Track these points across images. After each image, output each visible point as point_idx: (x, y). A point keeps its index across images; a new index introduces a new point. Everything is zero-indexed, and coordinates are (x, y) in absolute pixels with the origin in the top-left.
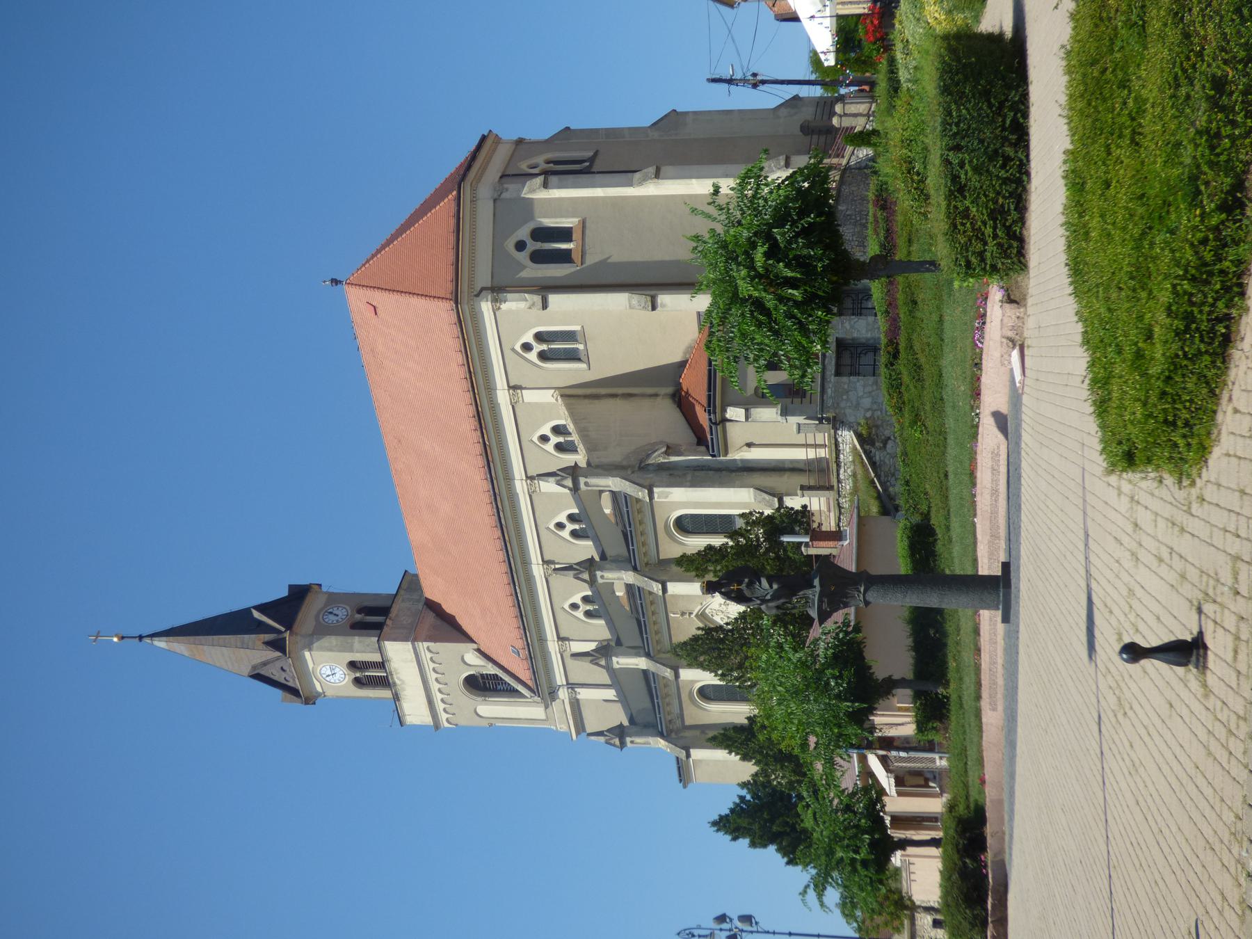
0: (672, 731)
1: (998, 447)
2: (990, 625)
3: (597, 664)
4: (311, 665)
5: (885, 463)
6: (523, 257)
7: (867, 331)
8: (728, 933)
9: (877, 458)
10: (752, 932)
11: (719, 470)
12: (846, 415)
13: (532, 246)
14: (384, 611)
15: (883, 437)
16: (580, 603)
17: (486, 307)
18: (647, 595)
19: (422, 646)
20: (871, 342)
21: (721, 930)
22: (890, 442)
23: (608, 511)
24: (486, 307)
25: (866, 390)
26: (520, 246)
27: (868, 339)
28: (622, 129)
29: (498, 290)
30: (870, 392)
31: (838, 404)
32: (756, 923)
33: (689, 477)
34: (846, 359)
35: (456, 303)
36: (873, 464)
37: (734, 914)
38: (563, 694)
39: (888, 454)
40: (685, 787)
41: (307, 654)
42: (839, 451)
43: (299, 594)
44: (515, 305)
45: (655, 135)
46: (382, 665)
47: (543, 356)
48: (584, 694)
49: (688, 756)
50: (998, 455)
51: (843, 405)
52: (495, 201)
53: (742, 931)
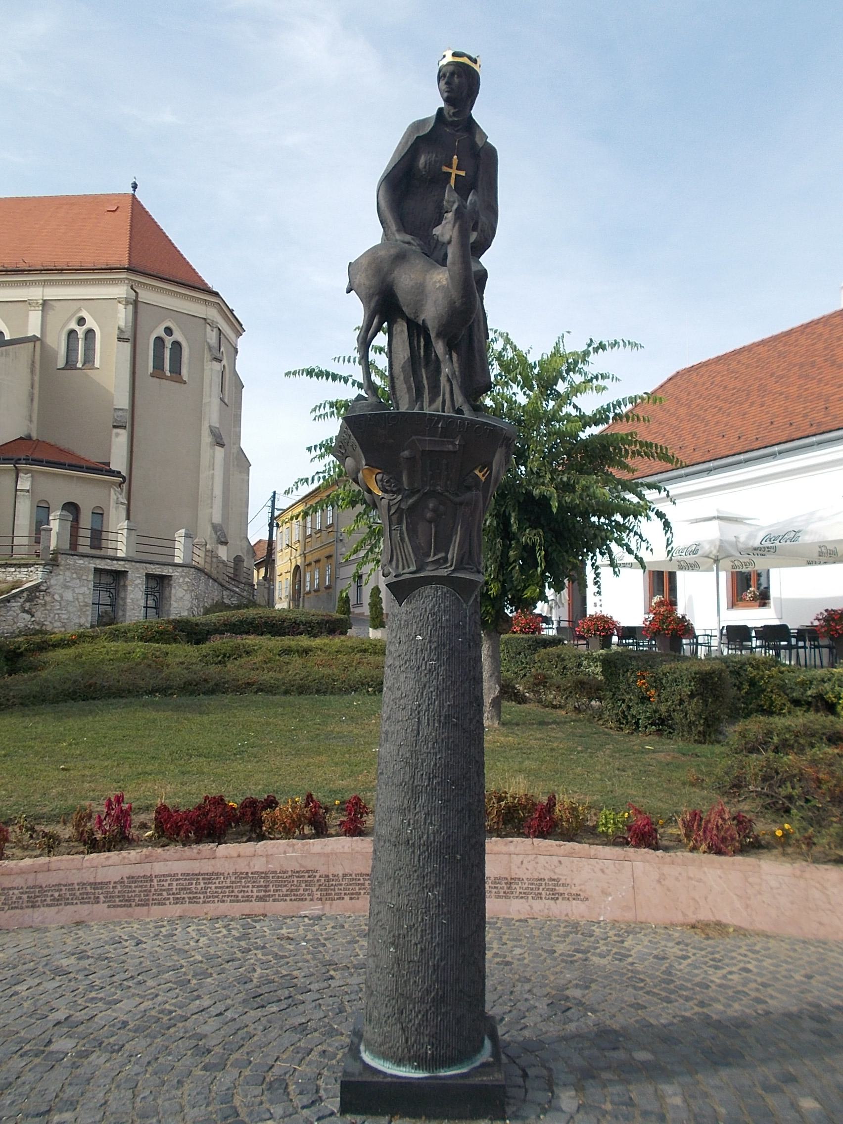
1: (577, 897)
2: (83, 884)
5: (8, 611)
6: (160, 332)
7: (131, 599)
12: (57, 576)
15: (34, 610)
20: (121, 602)
22: (29, 616)
24: (121, 291)
25: (81, 597)
27: (124, 599)
30: (77, 599)
31: (68, 569)
39: (18, 614)
42: (20, 567)
44: (122, 316)
45: (234, 450)
47: (72, 333)
50: (555, 896)
51: (68, 573)
52: (205, 319)
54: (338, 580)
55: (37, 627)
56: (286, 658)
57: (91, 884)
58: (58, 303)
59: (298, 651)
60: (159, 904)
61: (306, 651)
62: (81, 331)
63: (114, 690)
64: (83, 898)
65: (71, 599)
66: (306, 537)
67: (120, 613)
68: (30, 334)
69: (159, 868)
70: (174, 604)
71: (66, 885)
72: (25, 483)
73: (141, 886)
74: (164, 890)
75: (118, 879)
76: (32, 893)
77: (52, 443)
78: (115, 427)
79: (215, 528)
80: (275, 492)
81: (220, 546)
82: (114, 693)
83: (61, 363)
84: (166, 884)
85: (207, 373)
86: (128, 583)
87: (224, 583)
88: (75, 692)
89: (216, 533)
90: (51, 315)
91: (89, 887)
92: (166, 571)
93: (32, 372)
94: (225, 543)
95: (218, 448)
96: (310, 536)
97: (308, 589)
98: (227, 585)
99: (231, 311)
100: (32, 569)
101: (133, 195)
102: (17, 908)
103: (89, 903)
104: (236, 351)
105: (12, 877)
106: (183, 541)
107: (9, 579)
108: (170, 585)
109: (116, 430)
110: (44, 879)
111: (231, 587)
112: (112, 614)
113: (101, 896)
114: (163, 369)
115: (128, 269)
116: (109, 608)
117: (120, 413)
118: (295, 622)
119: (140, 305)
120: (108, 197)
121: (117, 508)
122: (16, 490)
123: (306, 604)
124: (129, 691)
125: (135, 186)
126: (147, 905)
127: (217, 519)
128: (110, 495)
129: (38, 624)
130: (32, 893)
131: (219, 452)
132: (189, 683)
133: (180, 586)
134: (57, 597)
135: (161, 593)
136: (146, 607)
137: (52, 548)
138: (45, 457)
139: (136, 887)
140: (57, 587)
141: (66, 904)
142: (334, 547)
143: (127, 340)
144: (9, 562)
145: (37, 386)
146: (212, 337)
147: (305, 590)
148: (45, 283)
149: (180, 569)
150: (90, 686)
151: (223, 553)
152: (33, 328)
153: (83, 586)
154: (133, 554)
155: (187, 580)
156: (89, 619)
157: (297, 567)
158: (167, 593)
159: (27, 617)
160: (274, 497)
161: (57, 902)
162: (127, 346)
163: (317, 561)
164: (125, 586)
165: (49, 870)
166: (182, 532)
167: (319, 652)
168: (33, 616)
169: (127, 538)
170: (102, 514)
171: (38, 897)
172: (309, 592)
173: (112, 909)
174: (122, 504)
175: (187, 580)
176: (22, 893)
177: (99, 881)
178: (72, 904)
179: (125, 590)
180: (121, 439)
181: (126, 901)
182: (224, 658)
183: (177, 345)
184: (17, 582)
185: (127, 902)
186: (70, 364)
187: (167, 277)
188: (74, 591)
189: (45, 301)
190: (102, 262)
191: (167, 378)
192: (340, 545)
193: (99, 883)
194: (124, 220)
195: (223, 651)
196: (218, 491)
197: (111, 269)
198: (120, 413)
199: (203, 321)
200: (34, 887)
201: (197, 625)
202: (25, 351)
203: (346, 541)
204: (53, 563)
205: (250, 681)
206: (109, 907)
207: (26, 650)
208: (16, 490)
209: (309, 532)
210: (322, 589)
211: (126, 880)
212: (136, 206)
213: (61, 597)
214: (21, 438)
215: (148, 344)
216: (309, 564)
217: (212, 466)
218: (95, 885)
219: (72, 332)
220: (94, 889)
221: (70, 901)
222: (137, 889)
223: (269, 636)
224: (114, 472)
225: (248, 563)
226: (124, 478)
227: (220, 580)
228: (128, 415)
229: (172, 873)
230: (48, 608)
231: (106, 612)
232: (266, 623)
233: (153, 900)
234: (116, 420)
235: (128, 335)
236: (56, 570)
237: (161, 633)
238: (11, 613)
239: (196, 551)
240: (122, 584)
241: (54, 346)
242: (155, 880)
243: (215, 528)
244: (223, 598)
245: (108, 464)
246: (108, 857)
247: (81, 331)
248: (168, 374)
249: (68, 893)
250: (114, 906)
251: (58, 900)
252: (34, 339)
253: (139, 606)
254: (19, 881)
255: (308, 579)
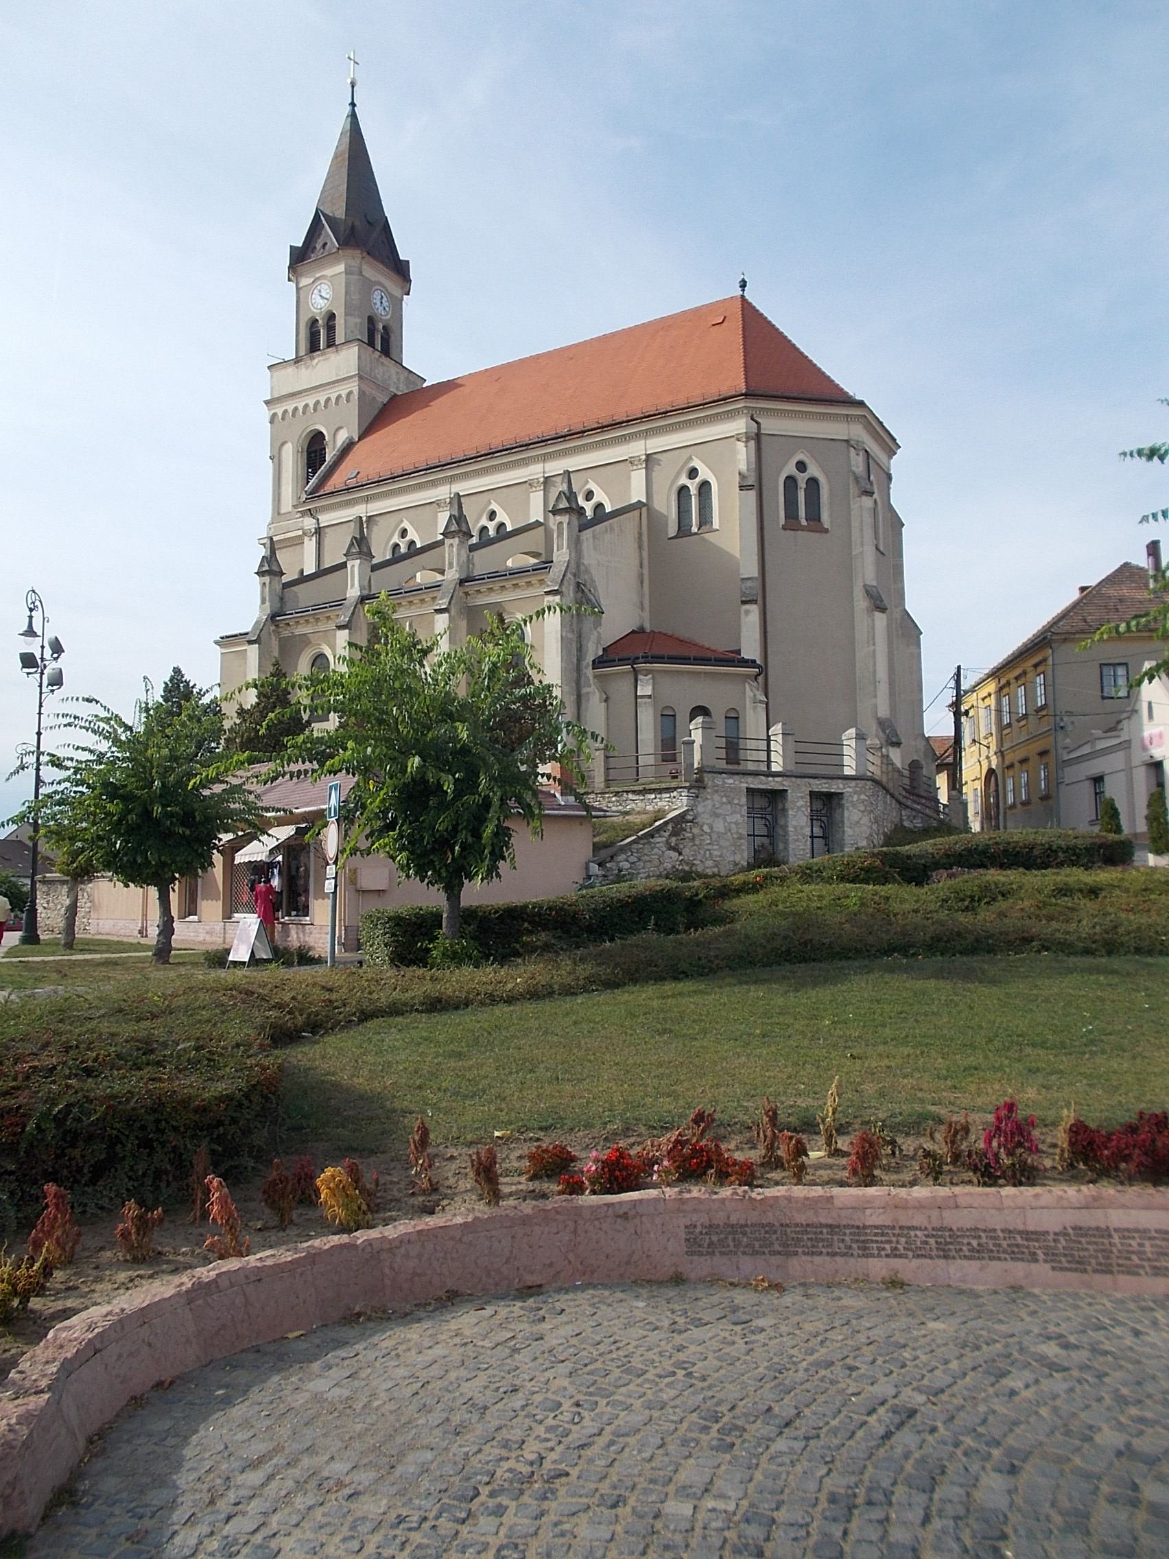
0: (277, 626)
3: (352, 544)
4: (329, 272)
5: (652, 849)
6: (790, 469)
7: (795, 827)
8: (38, 656)
9: (659, 840)
10: (41, 686)
11: (578, 669)
13: (802, 479)
14: (386, 351)
16: (408, 538)
17: (739, 425)
18: (431, 595)
19: (354, 386)
21: (43, 647)
23: (509, 563)
24: (739, 425)
26: (801, 466)
27: (785, 827)
28: (902, 581)
29: (757, 438)
31: (717, 791)
32: (52, 691)
33: (570, 636)
34: (760, 802)
35: (745, 395)
36: (651, 835)
37: (63, 662)
38: (309, 523)
40: (216, 642)
41: (341, 268)
43: (401, 270)
44: (742, 456)
45: (897, 615)
46: (331, 343)
48: (310, 545)
49: (250, 642)
51: (716, 797)
52: (847, 441)
53: (42, 673)
54: (1062, 787)
55: (687, 868)
56: (1065, 901)
57: (1020, 1232)
58: (664, 455)
59: (1081, 891)
60: (1129, 1273)
61: (1093, 892)
62: (693, 486)
63: (838, 949)
64: (1013, 1252)
65: (722, 830)
66: (1001, 728)
67: (781, 846)
68: (634, 501)
69: (1117, 1218)
70: (848, 831)
71: (985, 1231)
72: (645, 689)
73: (1096, 1243)
74: (1133, 1252)
75: (1058, 1229)
76: (941, 1237)
77: (670, 633)
78: (744, 602)
79: (882, 723)
80: (959, 668)
81: (891, 749)
82: (838, 953)
83: (672, 530)
84: (1133, 1243)
85: (855, 512)
86: (788, 805)
87: (901, 798)
88: (788, 951)
89: (884, 731)
90: (657, 473)
91: (1018, 1237)
92: (835, 787)
93: (640, 547)
94: (897, 744)
95: (878, 615)
96: (1009, 725)
97: (1010, 800)
98: (904, 800)
99: (881, 423)
100: (675, 793)
101: (743, 296)
102: (925, 1256)
103: (1022, 1260)
104: (889, 477)
105: (910, 1212)
106: (853, 744)
107: (649, 808)
108: (841, 806)
109: (747, 607)
110: (953, 1219)
111: (909, 803)
112: (770, 848)
113: (1039, 1252)
114: (797, 517)
115: (746, 395)
116: (766, 841)
117: (749, 584)
118: (1050, 849)
119: (764, 439)
120: (711, 307)
121: (755, 708)
122: (636, 697)
123: (1009, 824)
124: (857, 951)
125: (743, 285)
126: (1111, 1272)
127: (883, 711)
128: (744, 693)
129: (687, 864)
130: (941, 1237)
131: (880, 619)
132: (937, 939)
133: (854, 806)
134: (706, 828)
135: (830, 816)
136: (812, 837)
137: (696, 766)
138: (666, 652)
139: (1088, 1243)
140: (706, 816)
141: (991, 1259)
142: (1051, 739)
143: (750, 487)
144: (648, 787)
145: (646, 563)
146: (858, 463)
147: (1005, 803)
148: (647, 434)
149: (853, 783)
150: (805, 943)
151: (896, 755)
152: (637, 494)
153: (735, 812)
154: (792, 767)
155: (863, 797)
156: (745, 855)
157: (991, 772)
158: (837, 816)
159: (674, 854)
160: (958, 674)
161: (977, 1253)
162: (752, 495)
163: (1024, 761)
164: (784, 810)
165: (957, 1207)
166: (852, 732)
167: (1118, 892)
168: (680, 854)
169: (783, 746)
170: (737, 718)
171: (951, 1243)
172: (1013, 806)
173: (1058, 1273)
174: (761, 702)
175: (863, 797)
176: (927, 1236)
177: (1031, 1228)
178: (999, 1259)
179: (785, 815)
180: (751, 617)
181: (1078, 1262)
182: (972, 902)
183: (813, 482)
184: (659, 811)
185: (1079, 1265)
186: (683, 530)
187: (795, 395)
188: (725, 820)
189: (648, 456)
190: (713, 392)
191: (803, 529)
192: (1060, 735)
193: (1032, 1233)
194: (733, 334)
195: (969, 893)
196: (882, 673)
197: (725, 399)
198: (749, 584)
199: (845, 444)
200: (942, 1229)
201: (909, 857)
202: (631, 519)
203: (1070, 728)
204: (698, 785)
205: (1026, 935)
206: (1053, 1269)
207: (705, 897)
208: (636, 697)
209: (1006, 720)
210: (1035, 799)
211: (1070, 1231)
212: (747, 308)
213: (711, 828)
214: (633, 632)
215: (777, 488)
216: (1011, 766)
217: (872, 640)
218: (1027, 1235)
219: (683, 489)
220: (1027, 1240)
221: (996, 1255)
222: (1090, 1247)
223: (1021, 870)
224: (747, 661)
225: (927, 769)
226: (759, 667)
227: (897, 794)
228: (757, 585)
229: (1140, 1227)
230: (697, 842)
231: (763, 845)
232: (1005, 851)
233: (1119, 1265)
234: (744, 594)
235: (751, 481)
236: (703, 794)
237: (867, 870)
238: (656, 850)
239: (871, 757)
240: (780, 806)
241: (663, 510)
242: (1115, 1235)
243: (882, 723)
244: (901, 820)
245: (738, 652)
246: (1036, 1196)
247: (693, 486)
248: (804, 522)
249: (991, 1242)
250: (1062, 1269)
251: (978, 1251)
252: (538, 524)
253: (804, 836)
254: (919, 1219)
255: (1010, 786)
